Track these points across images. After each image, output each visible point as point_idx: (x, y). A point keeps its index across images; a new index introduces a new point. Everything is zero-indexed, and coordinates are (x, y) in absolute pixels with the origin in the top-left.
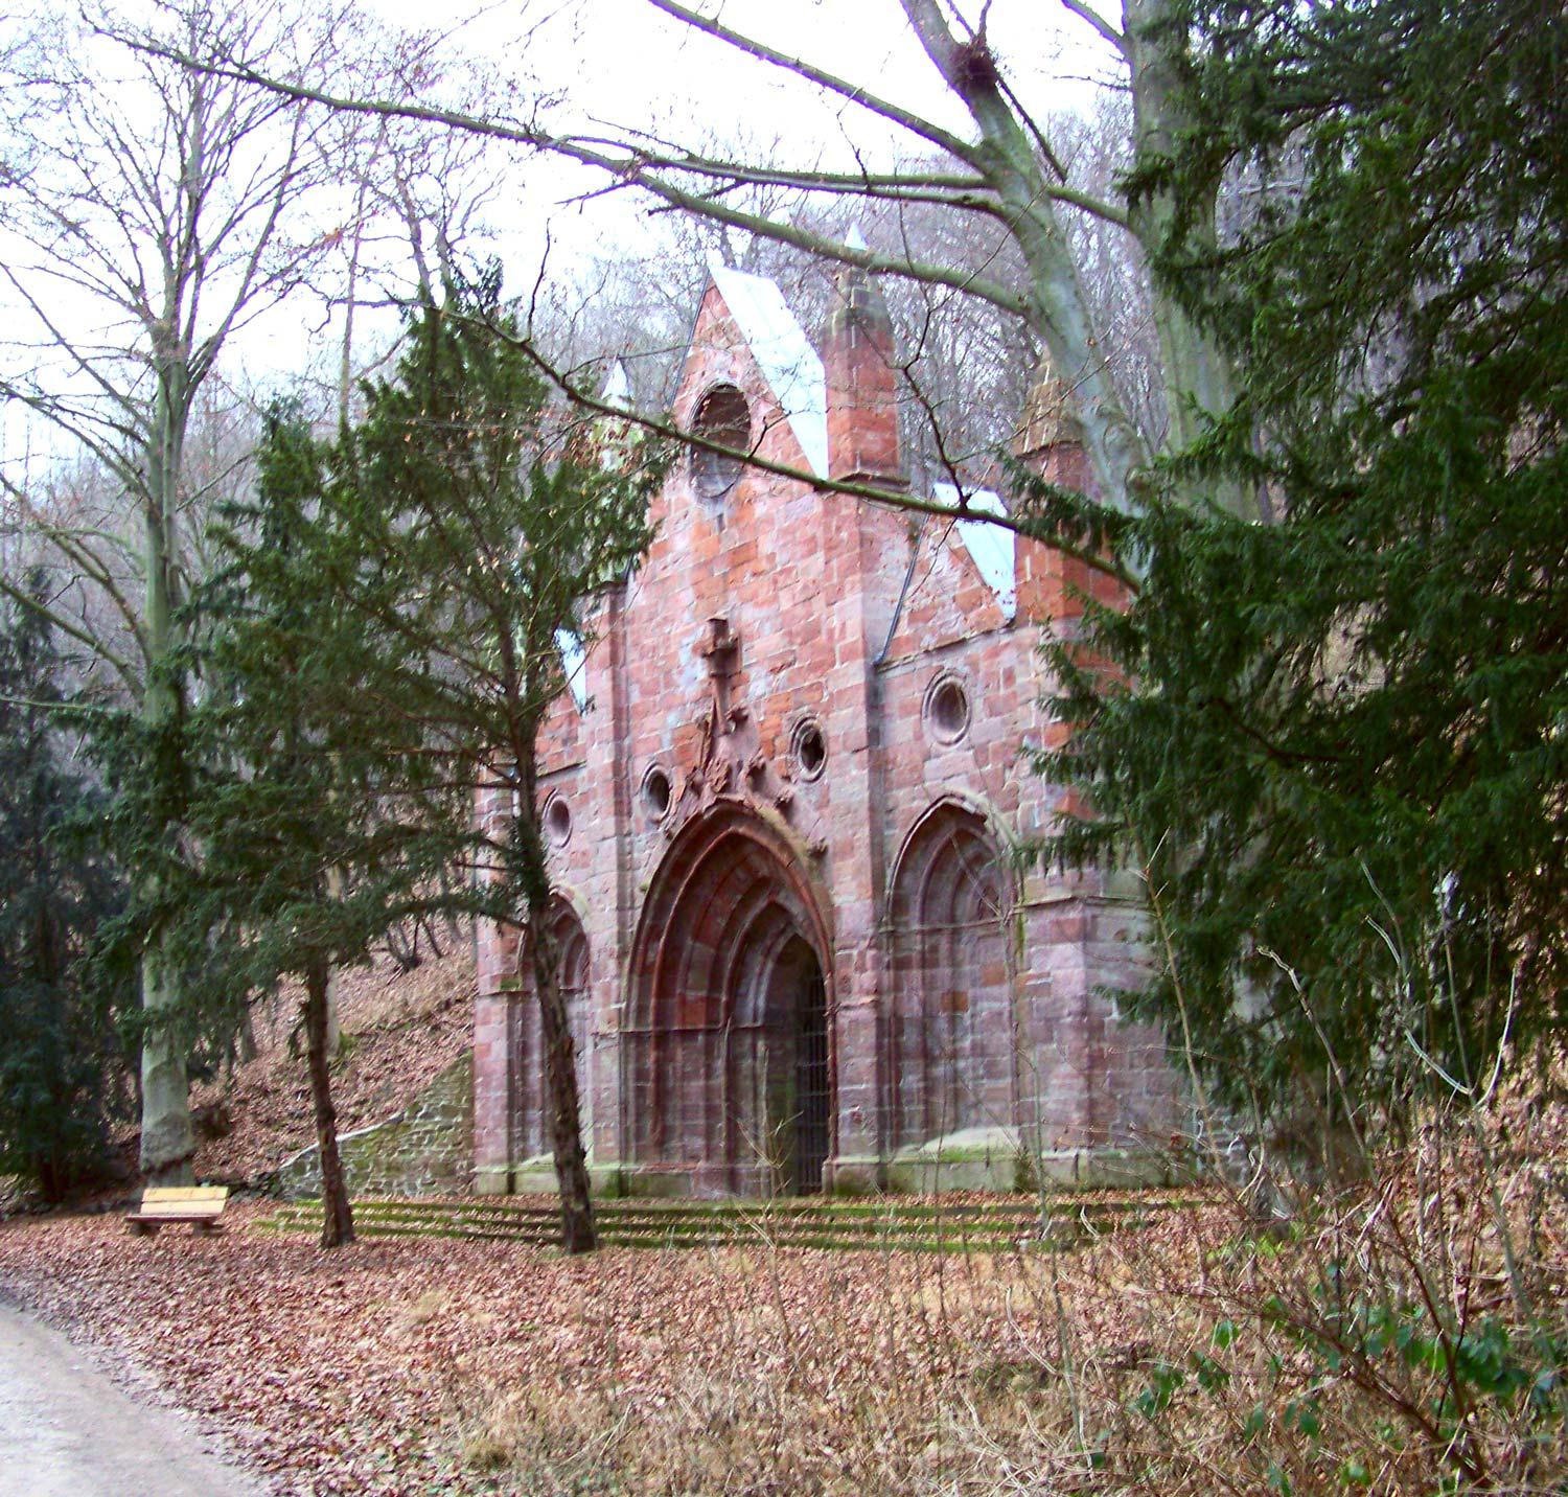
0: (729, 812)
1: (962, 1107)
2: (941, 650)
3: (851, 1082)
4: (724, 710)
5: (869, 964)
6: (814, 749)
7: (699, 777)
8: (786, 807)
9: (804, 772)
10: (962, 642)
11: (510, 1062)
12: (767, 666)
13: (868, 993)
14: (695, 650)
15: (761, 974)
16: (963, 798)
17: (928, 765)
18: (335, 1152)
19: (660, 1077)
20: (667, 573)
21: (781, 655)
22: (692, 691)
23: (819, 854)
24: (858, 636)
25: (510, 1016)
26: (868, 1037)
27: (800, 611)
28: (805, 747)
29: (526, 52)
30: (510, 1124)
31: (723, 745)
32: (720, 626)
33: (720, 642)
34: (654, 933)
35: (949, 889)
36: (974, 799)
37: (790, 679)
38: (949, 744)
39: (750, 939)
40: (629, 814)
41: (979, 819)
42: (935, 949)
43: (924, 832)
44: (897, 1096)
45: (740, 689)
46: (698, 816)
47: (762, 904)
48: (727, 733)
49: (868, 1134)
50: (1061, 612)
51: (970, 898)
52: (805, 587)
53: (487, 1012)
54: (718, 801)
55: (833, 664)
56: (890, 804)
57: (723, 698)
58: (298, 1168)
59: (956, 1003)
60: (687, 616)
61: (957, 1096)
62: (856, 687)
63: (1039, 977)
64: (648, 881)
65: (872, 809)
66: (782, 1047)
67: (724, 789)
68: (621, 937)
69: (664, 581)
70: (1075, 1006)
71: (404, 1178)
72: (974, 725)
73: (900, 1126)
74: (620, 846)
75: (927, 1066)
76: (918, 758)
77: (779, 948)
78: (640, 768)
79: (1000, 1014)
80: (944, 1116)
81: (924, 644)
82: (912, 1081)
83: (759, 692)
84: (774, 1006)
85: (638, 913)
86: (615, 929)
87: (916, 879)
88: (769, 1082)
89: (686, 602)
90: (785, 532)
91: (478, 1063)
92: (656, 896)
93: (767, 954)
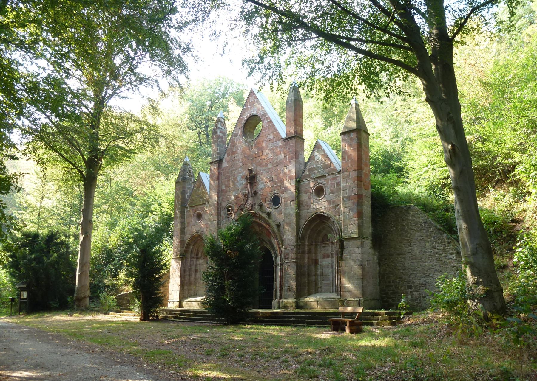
6: (276, 201)
8: (269, 214)
10: (325, 176)
14: (242, 177)
16: (324, 213)
23: (279, 226)
29: (200, 59)
32: (251, 171)
45: (255, 187)
48: (252, 196)
49: (293, 294)
51: (352, 230)
61: (316, 284)
74: (218, 223)
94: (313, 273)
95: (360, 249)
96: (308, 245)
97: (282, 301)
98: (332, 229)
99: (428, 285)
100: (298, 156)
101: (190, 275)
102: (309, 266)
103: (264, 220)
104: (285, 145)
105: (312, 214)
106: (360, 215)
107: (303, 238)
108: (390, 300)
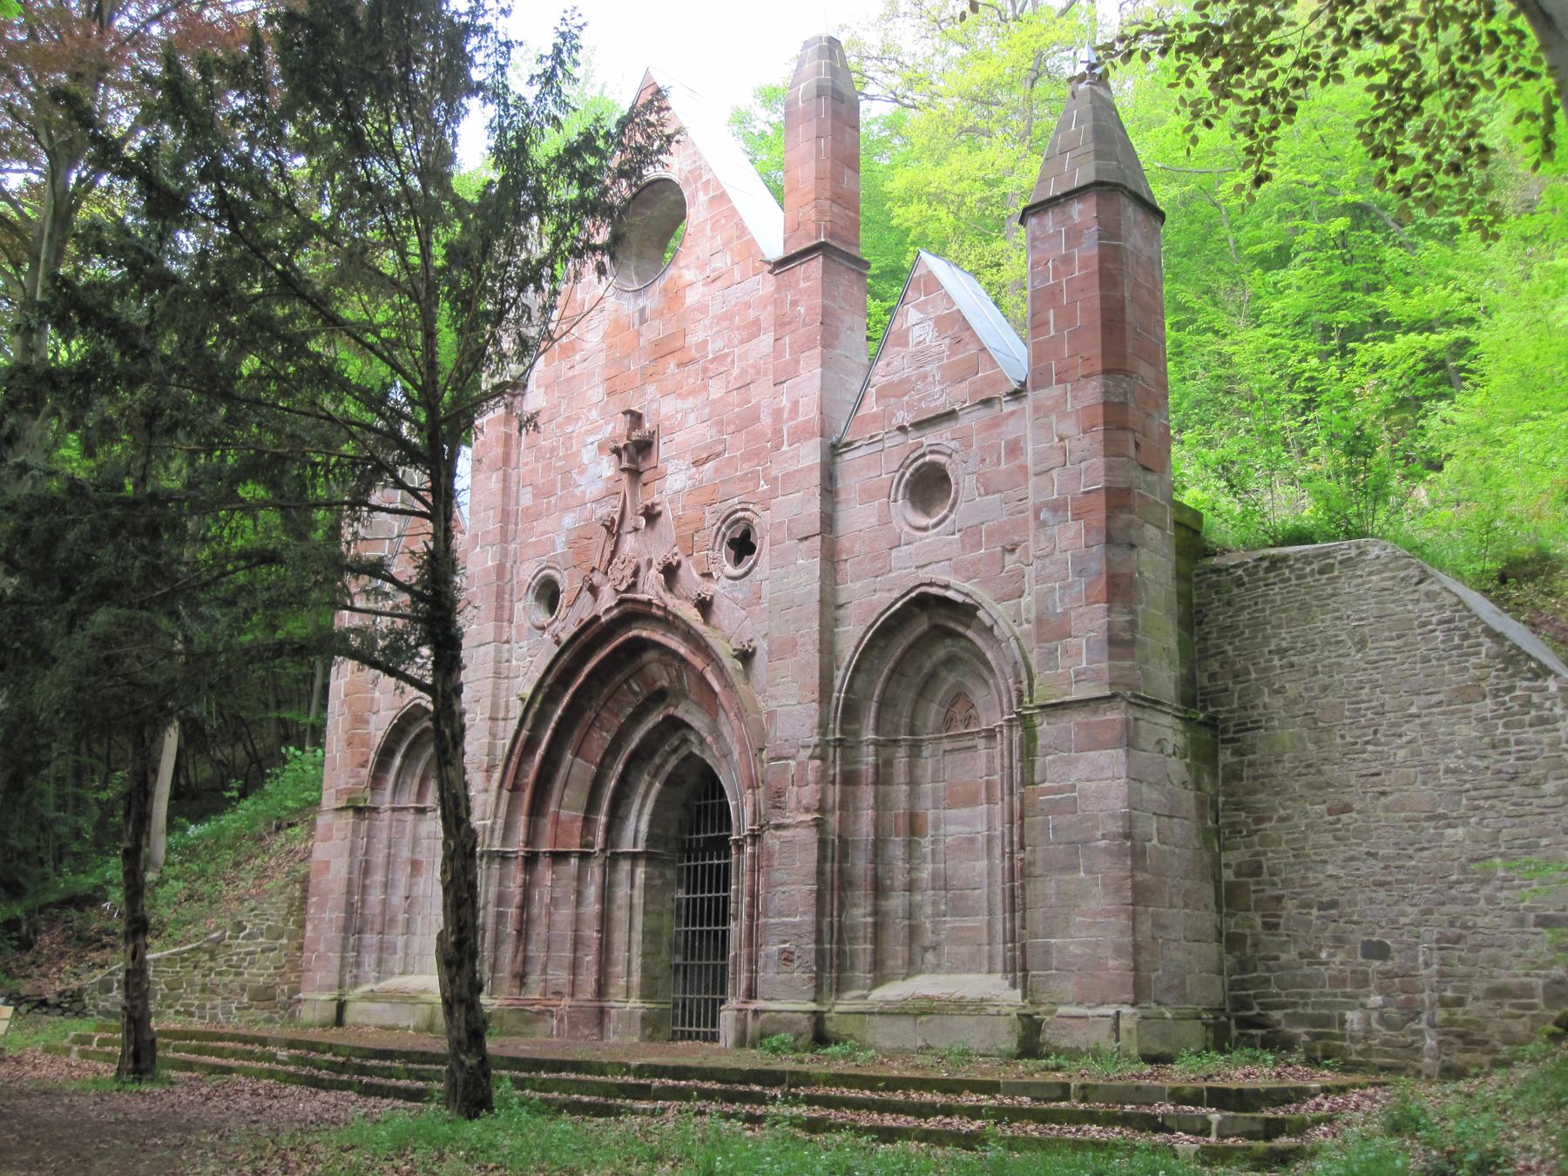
0: (633, 612)
1: (917, 949)
2: (919, 425)
3: (781, 914)
4: (634, 504)
5: (811, 776)
7: (597, 578)
9: (730, 570)
10: (950, 415)
11: (350, 880)
12: (689, 458)
13: (807, 810)
14: (601, 448)
15: (646, 796)
16: (947, 587)
17: (894, 553)
18: (143, 972)
19: (526, 902)
20: (576, 371)
21: (709, 446)
22: (595, 490)
23: (746, 657)
24: (814, 414)
25: (355, 832)
26: (807, 859)
27: (735, 397)
28: (732, 543)
30: (344, 949)
31: (629, 543)
33: (636, 435)
34: (530, 746)
35: (911, 695)
36: (959, 588)
37: (717, 470)
38: (925, 529)
39: (639, 758)
40: (510, 621)
41: (967, 611)
42: (889, 763)
43: (888, 629)
44: (842, 934)
46: (597, 618)
47: (655, 718)
49: (801, 976)
50: (1099, 367)
52: (743, 372)
53: (329, 828)
54: (621, 602)
55: (777, 447)
56: (842, 599)
57: (634, 494)
58: (105, 987)
59: (914, 827)
60: (594, 414)
61: (913, 933)
62: (810, 469)
63: (1060, 791)
64: (528, 691)
65: (822, 602)
66: (662, 875)
67: (632, 587)
68: (491, 753)
69: (569, 380)
70: (1116, 827)
71: (219, 1001)
72: (961, 506)
73: (841, 968)
74: (498, 651)
75: (876, 898)
76: (884, 545)
77: (669, 768)
78: (527, 573)
79: (972, 840)
80: (896, 961)
81: (896, 422)
82: (860, 914)
83: (678, 486)
84: (658, 831)
85: (514, 724)
86: (486, 740)
87: (872, 683)
88: (645, 913)
89: (595, 399)
90: (719, 319)
91: (313, 881)
92: (537, 705)
93: (655, 776)
94: (900, 879)
95: (1120, 753)
96: (876, 743)
97: (756, 1012)
98: (987, 664)
99: (1471, 940)
100: (836, 336)
101: (387, 886)
102: (879, 845)
103: (690, 636)
104: (778, 289)
105: (896, 594)
106: (1119, 589)
107: (851, 712)
108: (1277, 1015)
